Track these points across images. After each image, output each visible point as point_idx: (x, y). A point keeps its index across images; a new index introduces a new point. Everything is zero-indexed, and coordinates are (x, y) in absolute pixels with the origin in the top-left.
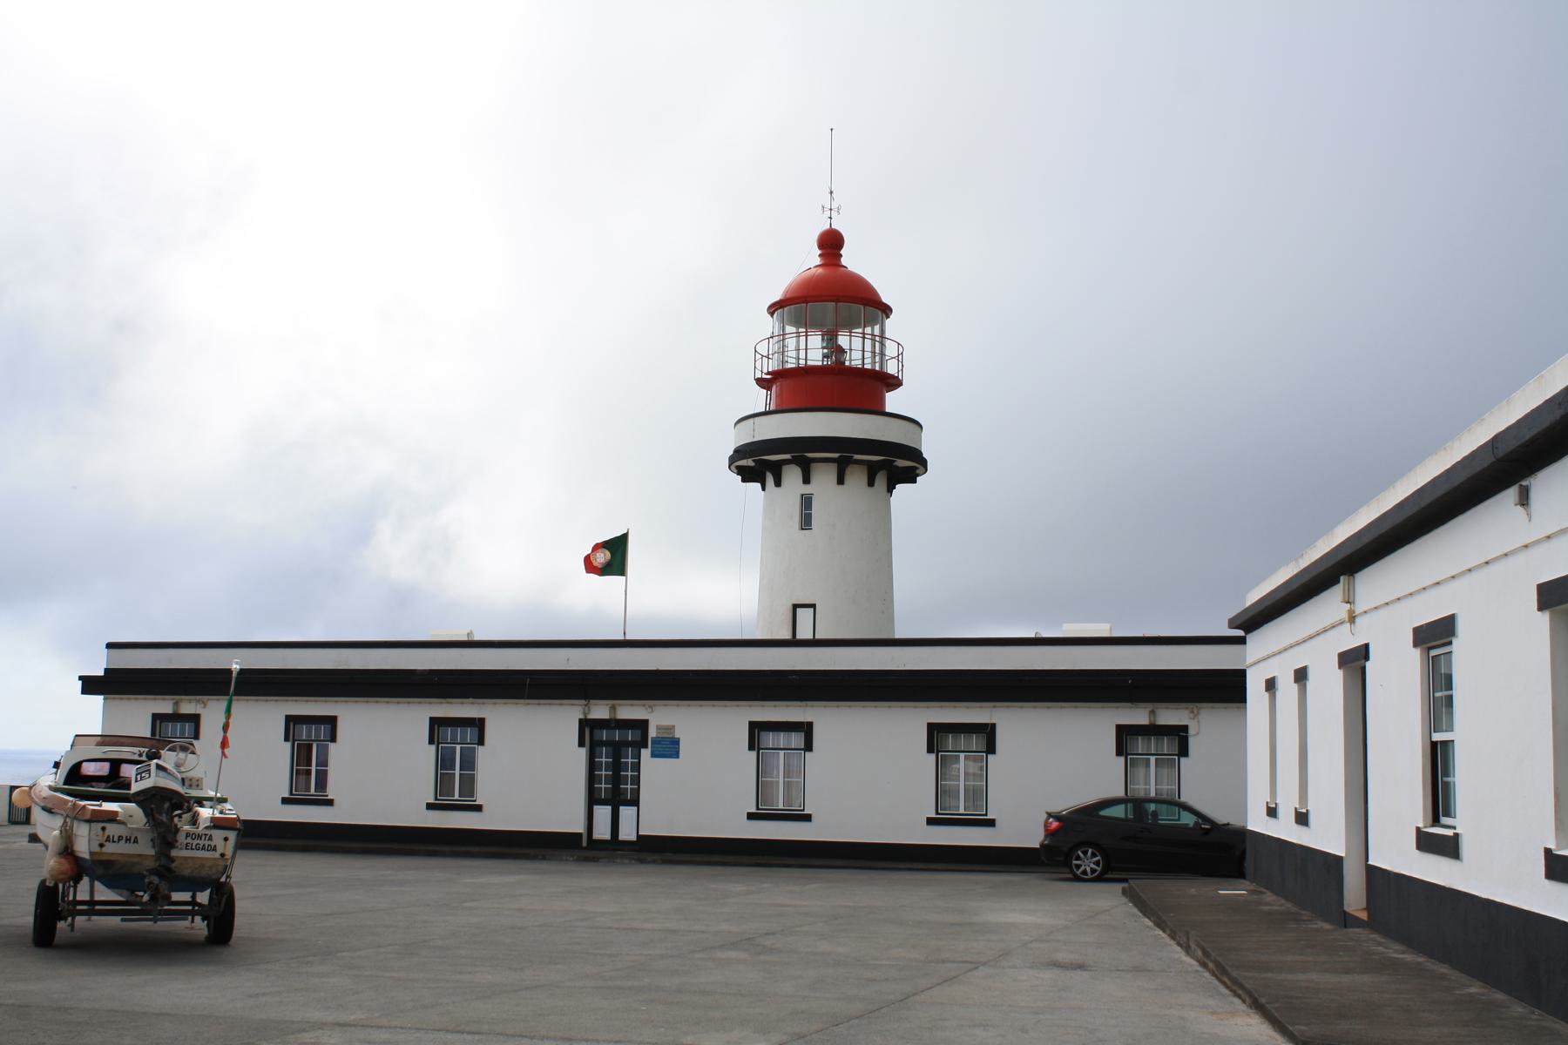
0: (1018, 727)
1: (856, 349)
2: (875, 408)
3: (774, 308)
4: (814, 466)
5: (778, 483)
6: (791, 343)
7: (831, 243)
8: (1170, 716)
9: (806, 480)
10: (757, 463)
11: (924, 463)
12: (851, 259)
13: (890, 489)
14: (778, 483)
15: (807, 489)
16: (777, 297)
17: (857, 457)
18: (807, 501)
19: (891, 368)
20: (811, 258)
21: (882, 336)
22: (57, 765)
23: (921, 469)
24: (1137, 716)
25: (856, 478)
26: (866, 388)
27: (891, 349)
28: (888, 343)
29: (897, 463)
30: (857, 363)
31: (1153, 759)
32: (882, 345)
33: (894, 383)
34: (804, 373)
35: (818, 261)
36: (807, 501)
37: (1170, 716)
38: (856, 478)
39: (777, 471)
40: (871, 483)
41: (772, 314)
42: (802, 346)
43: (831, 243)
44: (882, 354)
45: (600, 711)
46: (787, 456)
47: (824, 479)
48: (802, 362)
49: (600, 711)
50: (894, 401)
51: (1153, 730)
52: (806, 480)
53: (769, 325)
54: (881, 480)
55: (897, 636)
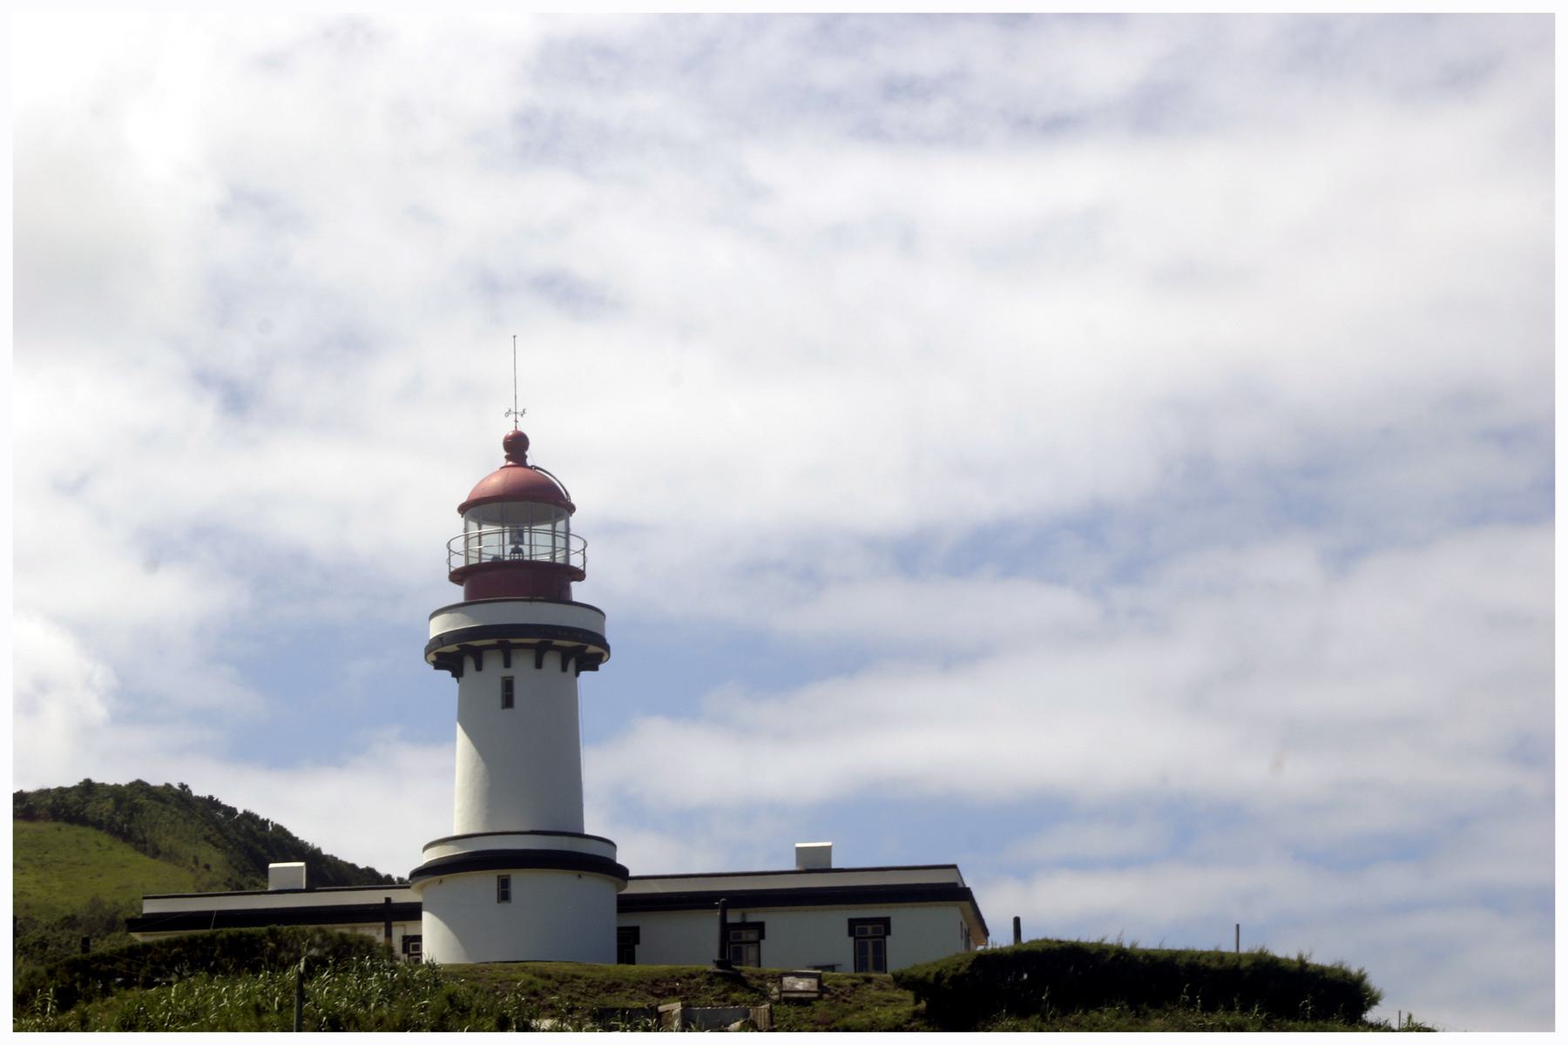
0: (902, 917)
1: (539, 545)
2: (561, 596)
3: (463, 509)
4: (486, 654)
5: (479, 668)
7: (516, 446)
8: (754, 916)
9: (507, 664)
10: (451, 655)
11: (607, 648)
13: (577, 675)
14: (479, 668)
15: (507, 673)
16: (464, 499)
17: (556, 642)
18: (508, 685)
19: (576, 561)
21: (567, 533)
22: (351, 38)
25: (552, 661)
26: (555, 579)
27: (576, 545)
28: (572, 539)
29: (584, 648)
31: (870, 942)
33: (579, 575)
34: (497, 564)
35: (503, 462)
36: (508, 685)
37: (754, 916)
38: (552, 661)
39: (478, 656)
40: (539, 665)
43: (516, 446)
44: (567, 549)
45: (734, 917)
46: (492, 642)
47: (522, 667)
48: (560, 525)
49: (734, 917)
50: (578, 592)
51: (744, 926)
52: (507, 664)
53: (459, 521)
54: (572, 665)
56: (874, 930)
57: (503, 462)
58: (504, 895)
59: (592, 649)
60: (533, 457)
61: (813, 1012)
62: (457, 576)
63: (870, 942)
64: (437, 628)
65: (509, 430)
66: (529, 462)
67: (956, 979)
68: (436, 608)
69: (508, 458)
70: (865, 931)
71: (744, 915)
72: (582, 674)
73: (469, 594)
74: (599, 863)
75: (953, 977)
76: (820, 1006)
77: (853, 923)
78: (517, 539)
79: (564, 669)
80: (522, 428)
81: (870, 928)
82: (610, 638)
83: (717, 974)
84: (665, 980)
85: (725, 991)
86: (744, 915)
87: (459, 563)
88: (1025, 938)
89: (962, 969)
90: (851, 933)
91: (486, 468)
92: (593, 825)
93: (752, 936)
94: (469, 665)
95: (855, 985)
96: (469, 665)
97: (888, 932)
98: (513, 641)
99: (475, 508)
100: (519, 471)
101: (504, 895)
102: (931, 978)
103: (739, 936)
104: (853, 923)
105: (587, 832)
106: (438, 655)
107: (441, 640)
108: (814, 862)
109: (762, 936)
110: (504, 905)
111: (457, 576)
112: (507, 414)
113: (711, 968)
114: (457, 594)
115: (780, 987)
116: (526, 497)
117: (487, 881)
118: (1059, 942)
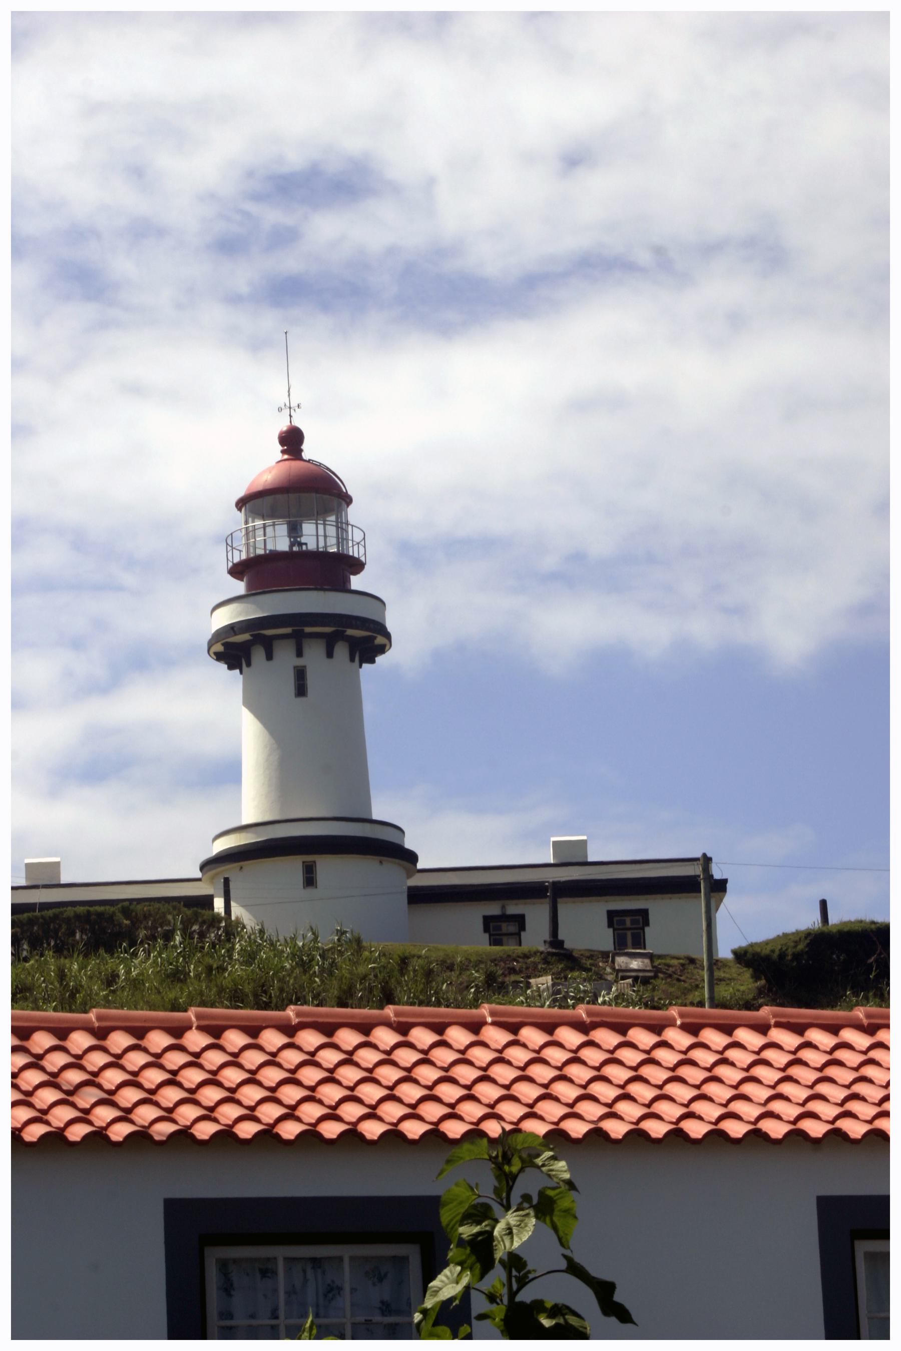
1: (315, 536)
2: (343, 587)
3: (241, 503)
5: (269, 657)
6: (332, 541)
7: (292, 441)
8: (513, 909)
9: (299, 654)
11: (388, 636)
12: (312, 450)
13: (361, 666)
14: (269, 657)
15: (300, 662)
16: (241, 493)
17: (308, 630)
18: (300, 675)
20: (275, 451)
23: (380, 640)
24: (493, 909)
25: (341, 651)
26: (338, 568)
29: (366, 638)
30: (312, 546)
31: (629, 934)
32: (338, 534)
33: (357, 566)
34: (274, 557)
35: (280, 456)
36: (300, 675)
37: (513, 909)
38: (341, 651)
40: (330, 654)
41: (240, 510)
42: (321, 539)
43: (292, 441)
47: (314, 655)
50: (357, 582)
51: (505, 918)
52: (299, 654)
53: (240, 516)
55: (62, 882)
56: (632, 922)
57: (280, 456)
58: (310, 880)
59: (380, 640)
60: (309, 451)
61: (654, 989)
62: (237, 571)
63: (629, 934)
64: (224, 618)
65: (284, 426)
66: (306, 455)
67: (797, 956)
68: (216, 603)
69: (283, 452)
70: (624, 922)
71: (503, 907)
72: (364, 665)
73: (249, 587)
74: (390, 850)
75: (794, 955)
76: (661, 983)
77: (611, 914)
78: (294, 530)
79: (352, 660)
80: (297, 423)
81: (628, 920)
82: (391, 625)
83: (549, 953)
84: (502, 959)
85: (563, 970)
86: (503, 907)
87: (239, 556)
88: (834, 919)
89: (801, 947)
90: (610, 924)
91: (264, 464)
92: (382, 809)
93: (512, 928)
94: (258, 655)
95: (683, 965)
96: (258, 655)
97: (647, 923)
98: (308, 630)
99: (253, 502)
100: (296, 464)
101: (310, 880)
102: (775, 956)
103: (500, 928)
104: (611, 914)
105: (375, 817)
106: (226, 645)
107: (232, 629)
108: (571, 855)
109: (522, 927)
110: (310, 891)
111: (237, 571)
112: (280, 410)
113: (542, 948)
114: (239, 587)
115: (613, 969)
116: (305, 491)
117: (293, 866)
118: (873, 923)
